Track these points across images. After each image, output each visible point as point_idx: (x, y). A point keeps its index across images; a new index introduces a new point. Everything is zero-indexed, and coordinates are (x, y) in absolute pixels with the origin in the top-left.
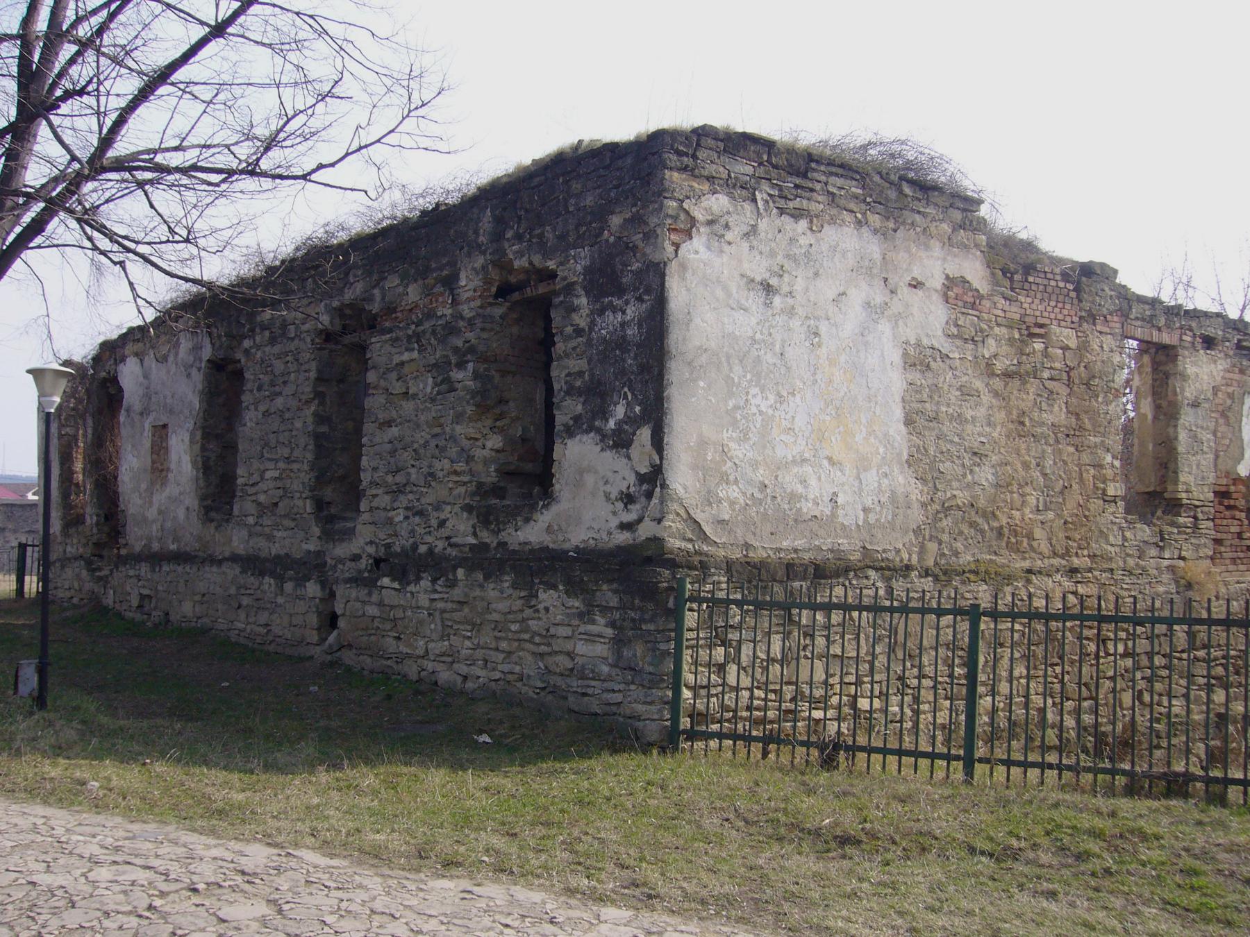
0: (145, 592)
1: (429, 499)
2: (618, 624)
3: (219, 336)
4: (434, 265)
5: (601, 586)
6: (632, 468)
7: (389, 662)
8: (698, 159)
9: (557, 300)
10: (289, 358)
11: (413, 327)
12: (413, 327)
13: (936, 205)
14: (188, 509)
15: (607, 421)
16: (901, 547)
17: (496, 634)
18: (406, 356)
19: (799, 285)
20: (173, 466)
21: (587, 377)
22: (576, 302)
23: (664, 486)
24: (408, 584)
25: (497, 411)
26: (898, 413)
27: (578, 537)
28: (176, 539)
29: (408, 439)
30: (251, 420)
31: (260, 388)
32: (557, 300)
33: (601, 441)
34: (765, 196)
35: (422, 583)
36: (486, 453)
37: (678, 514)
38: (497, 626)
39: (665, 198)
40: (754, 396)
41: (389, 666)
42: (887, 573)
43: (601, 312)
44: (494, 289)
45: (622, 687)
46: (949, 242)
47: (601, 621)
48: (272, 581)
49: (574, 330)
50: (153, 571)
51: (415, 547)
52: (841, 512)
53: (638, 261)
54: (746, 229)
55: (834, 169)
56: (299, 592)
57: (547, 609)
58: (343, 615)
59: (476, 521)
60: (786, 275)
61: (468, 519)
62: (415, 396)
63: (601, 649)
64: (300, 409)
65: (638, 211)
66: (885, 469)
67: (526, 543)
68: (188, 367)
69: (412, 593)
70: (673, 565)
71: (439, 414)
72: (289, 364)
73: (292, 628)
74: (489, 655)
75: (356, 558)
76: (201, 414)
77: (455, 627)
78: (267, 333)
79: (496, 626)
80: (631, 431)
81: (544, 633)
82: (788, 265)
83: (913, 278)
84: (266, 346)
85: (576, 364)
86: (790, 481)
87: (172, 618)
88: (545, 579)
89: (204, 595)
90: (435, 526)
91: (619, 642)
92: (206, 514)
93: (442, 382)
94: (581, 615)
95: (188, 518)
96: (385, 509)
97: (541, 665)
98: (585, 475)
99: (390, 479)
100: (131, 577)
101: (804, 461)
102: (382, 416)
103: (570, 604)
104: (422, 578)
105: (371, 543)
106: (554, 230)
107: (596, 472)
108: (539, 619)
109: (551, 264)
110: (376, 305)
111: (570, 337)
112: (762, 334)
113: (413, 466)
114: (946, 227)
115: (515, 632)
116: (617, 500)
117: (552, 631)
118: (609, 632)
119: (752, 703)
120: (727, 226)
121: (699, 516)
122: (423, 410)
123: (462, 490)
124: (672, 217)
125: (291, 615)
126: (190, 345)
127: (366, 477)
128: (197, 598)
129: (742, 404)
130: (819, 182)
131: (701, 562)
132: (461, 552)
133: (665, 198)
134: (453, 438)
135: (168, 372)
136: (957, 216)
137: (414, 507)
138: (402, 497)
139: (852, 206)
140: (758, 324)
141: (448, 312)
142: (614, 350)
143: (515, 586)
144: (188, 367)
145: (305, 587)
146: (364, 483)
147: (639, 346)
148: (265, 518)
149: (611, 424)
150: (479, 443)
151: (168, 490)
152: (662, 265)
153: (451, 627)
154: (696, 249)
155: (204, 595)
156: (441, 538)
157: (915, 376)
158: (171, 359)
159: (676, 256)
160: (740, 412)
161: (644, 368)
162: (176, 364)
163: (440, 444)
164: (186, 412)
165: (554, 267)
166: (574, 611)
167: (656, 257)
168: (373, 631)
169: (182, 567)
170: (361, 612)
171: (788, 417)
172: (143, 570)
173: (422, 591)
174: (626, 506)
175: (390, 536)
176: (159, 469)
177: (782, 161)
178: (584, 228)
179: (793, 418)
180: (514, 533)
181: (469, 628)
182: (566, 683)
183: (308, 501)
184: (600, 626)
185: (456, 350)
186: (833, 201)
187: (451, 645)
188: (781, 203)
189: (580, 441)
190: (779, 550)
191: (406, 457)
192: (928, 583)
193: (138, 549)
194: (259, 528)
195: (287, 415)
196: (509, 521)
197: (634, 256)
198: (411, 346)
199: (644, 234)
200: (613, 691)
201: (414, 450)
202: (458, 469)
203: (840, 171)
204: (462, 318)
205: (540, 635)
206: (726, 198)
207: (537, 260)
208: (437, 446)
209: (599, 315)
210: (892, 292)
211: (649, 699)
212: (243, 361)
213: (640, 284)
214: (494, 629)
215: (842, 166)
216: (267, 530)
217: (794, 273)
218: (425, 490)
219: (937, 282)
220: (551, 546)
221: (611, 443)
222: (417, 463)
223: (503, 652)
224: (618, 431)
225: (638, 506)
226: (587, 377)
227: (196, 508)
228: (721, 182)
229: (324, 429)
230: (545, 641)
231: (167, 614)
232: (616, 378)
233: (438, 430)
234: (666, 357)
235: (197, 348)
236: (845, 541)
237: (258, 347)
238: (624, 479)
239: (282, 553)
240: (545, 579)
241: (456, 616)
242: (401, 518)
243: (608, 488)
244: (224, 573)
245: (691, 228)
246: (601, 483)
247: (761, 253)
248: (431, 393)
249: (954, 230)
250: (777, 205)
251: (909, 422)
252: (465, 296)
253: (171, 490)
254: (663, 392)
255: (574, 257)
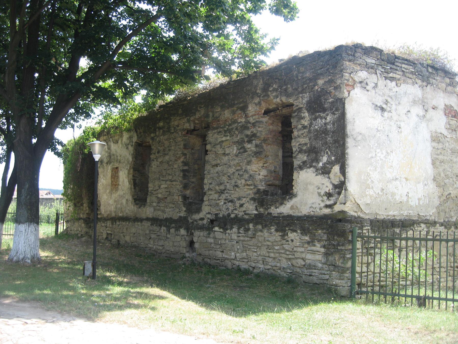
0: (109, 232)
1: (237, 195)
2: (327, 246)
3: (140, 133)
4: (236, 102)
5: (318, 231)
6: (331, 182)
7: (218, 261)
8: (355, 57)
9: (294, 115)
10: (171, 140)
11: (227, 127)
12: (227, 127)
13: (441, 76)
14: (127, 200)
15: (319, 163)
16: (432, 214)
17: (268, 250)
18: (224, 139)
19: (394, 107)
20: (120, 183)
21: (308, 145)
22: (303, 115)
23: (346, 190)
24: (227, 229)
25: (265, 160)
26: (429, 160)
27: (305, 211)
28: (122, 212)
29: (225, 172)
30: (154, 165)
31: (158, 152)
32: (294, 115)
33: (316, 171)
34: (380, 72)
35: (234, 230)
36: (261, 177)
37: (351, 201)
38: (268, 247)
39: (344, 72)
40: (378, 153)
41: (218, 263)
42: (428, 225)
43: (315, 119)
44: (263, 111)
45: (328, 272)
46: (445, 91)
47: (318, 245)
48: (165, 228)
49: (302, 127)
50: (112, 224)
51: (229, 215)
52: (410, 200)
53: (332, 98)
54: (374, 85)
55: (404, 62)
56: (177, 233)
57: (292, 241)
58: (197, 242)
59: (257, 204)
60: (388, 104)
61: (253, 204)
62: (228, 154)
63: (319, 257)
64: (176, 160)
65: (331, 78)
66: (426, 182)
67: (281, 213)
68: (127, 145)
69: (229, 233)
70: (350, 222)
71: (240, 162)
72: (171, 143)
73: (174, 247)
74: (265, 259)
75: (202, 219)
76: (133, 163)
77: (249, 247)
78: (161, 131)
79: (268, 247)
80: (330, 167)
81: (291, 250)
82: (389, 100)
83: (433, 105)
84: (161, 136)
85: (303, 140)
86: (391, 187)
87: (120, 243)
88: (291, 228)
89: (134, 234)
90: (238, 206)
91: (326, 254)
92: (135, 202)
93: (241, 148)
94: (308, 243)
95: (127, 203)
96: (215, 200)
97: (289, 263)
98: (308, 185)
99: (217, 188)
100: (103, 226)
101: (397, 179)
102: (214, 163)
103: (303, 238)
104: (234, 228)
105: (209, 213)
106: (292, 86)
107: (313, 184)
108: (289, 244)
109: (291, 101)
110: (210, 119)
111: (300, 129)
112: (380, 127)
113: (228, 182)
114: (444, 85)
115: (278, 250)
116: (324, 195)
117: (295, 249)
118: (323, 250)
119: (380, 279)
120: (367, 84)
121: (359, 202)
122: (232, 160)
123: (251, 192)
124: (347, 80)
125: (173, 242)
126: (128, 136)
127: (206, 187)
128: (131, 235)
129: (374, 156)
130: (399, 66)
131: (361, 221)
132: (250, 217)
133: (344, 72)
134: (246, 171)
135: (119, 147)
136: (448, 80)
137: (228, 199)
138: (223, 195)
139: (411, 76)
140: (379, 123)
141: (243, 120)
142: (321, 134)
143: (277, 230)
144: (127, 145)
145: (180, 231)
146: (206, 189)
147: (333, 132)
148: (161, 204)
149: (321, 164)
150: (257, 173)
151: (118, 193)
152: (343, 99)
153: (247, 247)
154: (357, 92)
155: (134, 234)
156: (241, 211)
157: (435, 144)
158: (120, 142)
159: (349, 96)
160: (373, 159)
161: (336, 141)
162: (122, 144)
163: (240, 173)
164: (126, 162)
165: (292, 101)
166: (305, 241)
167: (340, 96)
168: (211, 249)
169: (125, 222)
170: (205, 241)
171: (391, 161)
172: (108, 223)
173: (234, 232)
174: (328, 198)
175: (218, 210)
176: (115, 185)
177: (385, 58)
178: (306, 86)
179: (392, 162)
180: (275, 209)
181: (255, 248)
182: (302, 271)
183: (180, 197)
184: (318, 247)
185: (247, 136)
186: (404, 74)
187: (247, 255)
188: (386, 75)
189: (306, 171)
190: (388, 216)
191: (225, 179)
192: (442, 229)
193: (105, 216)
194: (158, 208)
195: (170, 163)
196: (273, 204)
197: (330, 96)
198: (226, 134)
199: (335, 87)
200: (324, 274)
201: (228, 176)
202: (249, 183)
203: (406, 62)
204: (250, 123)
205: (289, 251)
206: (366, 73)
207: (284, 99)
208: (239, 174)
209: (314, 120)
210: (426, 111)
211: (342, 278)
212: (151, 142)
213: (333, 107)
214: (267, 249)
215: (406, 60)
216: (162, 208)
217: (391, 103)
218: (233, 192)
219: (442, 106)
220: (293, 214)
221: (321, 172)
222: (230, 181)
223: (271, 257)
224: (324, 167)
225: (334, 198)
226: (308, 145)
227: (131, 199)
228: (364, 66)
229: (186, 168)
230: (292, 253)
231: (119, 241)
232: (323, 146)
233: (239, 168)
234: (346, 137)
235: (130, 138)
236: (412, 212)
237: (158, 136)
238: (327, 187)
239: (168, 217)
240: (291, 228)
241: (250, 243)
242: (223, 203)
243: (319, 191)
244: (143, 225)
245: (354, 85)
246: (316, 189)
247: (379, 95)
248: (236, 153)
249: (447, 86)
250: (384, 76)
251: (433, 163)
252: (250, 114)
253: (120, 192)
254: (345, 151)
255: (302, 97)
